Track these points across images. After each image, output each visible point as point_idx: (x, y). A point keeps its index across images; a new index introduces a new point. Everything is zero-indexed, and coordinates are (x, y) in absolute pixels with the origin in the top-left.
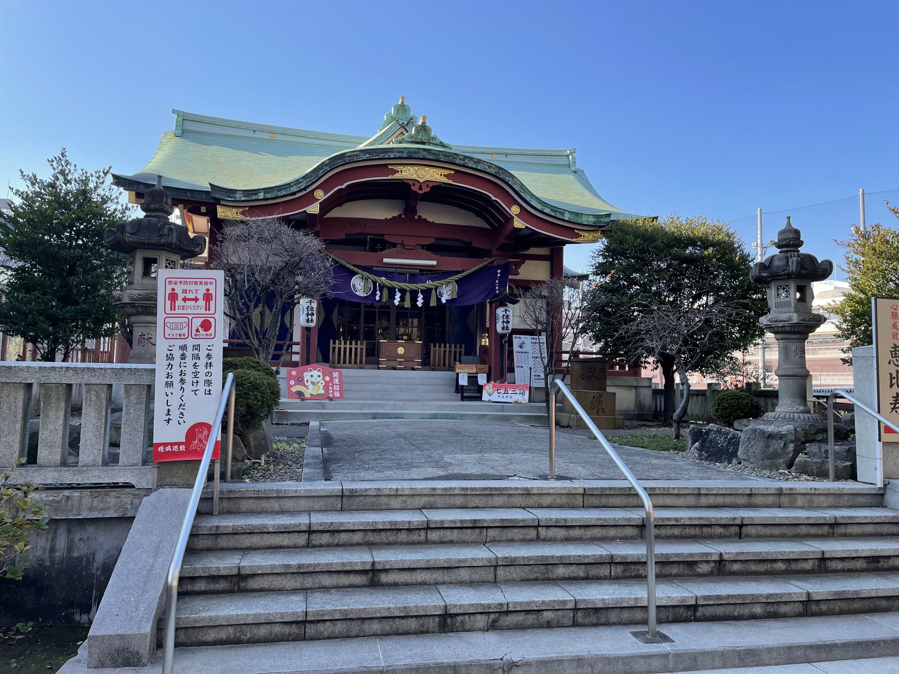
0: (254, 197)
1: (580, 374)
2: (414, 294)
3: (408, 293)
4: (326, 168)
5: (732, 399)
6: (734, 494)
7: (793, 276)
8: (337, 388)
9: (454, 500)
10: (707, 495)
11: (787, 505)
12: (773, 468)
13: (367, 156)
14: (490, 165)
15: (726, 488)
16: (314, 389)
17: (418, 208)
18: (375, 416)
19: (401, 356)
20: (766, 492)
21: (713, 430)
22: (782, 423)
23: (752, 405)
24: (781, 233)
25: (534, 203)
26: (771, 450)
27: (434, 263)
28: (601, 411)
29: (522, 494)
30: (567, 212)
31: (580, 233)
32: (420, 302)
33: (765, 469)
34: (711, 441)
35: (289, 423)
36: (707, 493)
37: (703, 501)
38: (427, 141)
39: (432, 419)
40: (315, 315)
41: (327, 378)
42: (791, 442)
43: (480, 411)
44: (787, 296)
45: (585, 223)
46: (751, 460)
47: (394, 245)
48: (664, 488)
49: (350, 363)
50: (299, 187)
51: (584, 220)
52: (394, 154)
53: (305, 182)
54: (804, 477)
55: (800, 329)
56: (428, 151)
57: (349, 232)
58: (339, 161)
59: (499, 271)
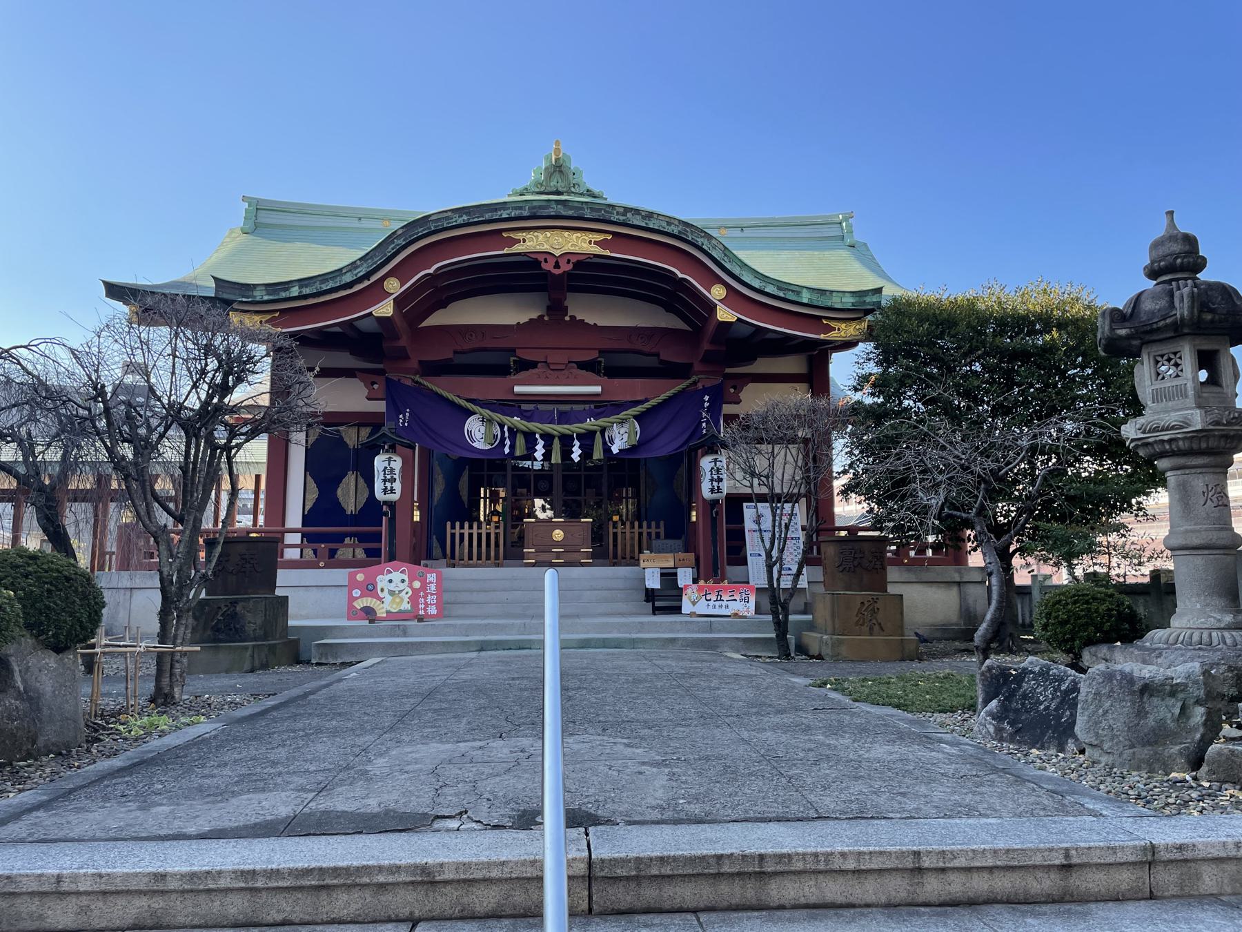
0: (283, 295)
1: (837, 564)
2: (566, 441)
3: (556, 441)
4: (399, 242)
5: (1075, 602)
6: (1021, 867)
7: (1186, 331)
8: (432, 599)
9: (222, 905)
10: (943, 870)
11: (1174, 890)
12: (1156, 766)
13: (465, 217)
14: (670, 220)
15: (995, 852)
16: (393, 601)
17: (566, 303)
18: (483, 646)
19: (558, 544)
20: (1111, 860)
21: (1031, 672)
22: (1182, 655)
23: (1119, 613)
24: (1156, 245)
25: (747, 278)
26: (1151, 721)
27: (598, 389)
28: (876, 628)
29: (412, 883)
30: (805, 290)
31: (832, 324)
32: (576, 454)
33: (1138, 768)
34: (1025, 696)
35: (339, 661)
36: (941, 865)
37: (932, 887)
38: (565, 189)
39: (582, 648)
40: (398, 480)
41: (417, 584)
42: (1198, 702)
43: (672, 631)
44: (1177, 376)
45: (837, 306)
46: (1106, 746)
47: (532, 365)
48: (816, 855)
49: (479, 558)
50: (356, 275)
51: (836, 302)
52: (508, 212)
53: (365, 265)
54: (1231, 791)
55: (1210, 444)
56: (564, 202)
57: (459, 348)
58: (420, 230)
59: (707, 398)
